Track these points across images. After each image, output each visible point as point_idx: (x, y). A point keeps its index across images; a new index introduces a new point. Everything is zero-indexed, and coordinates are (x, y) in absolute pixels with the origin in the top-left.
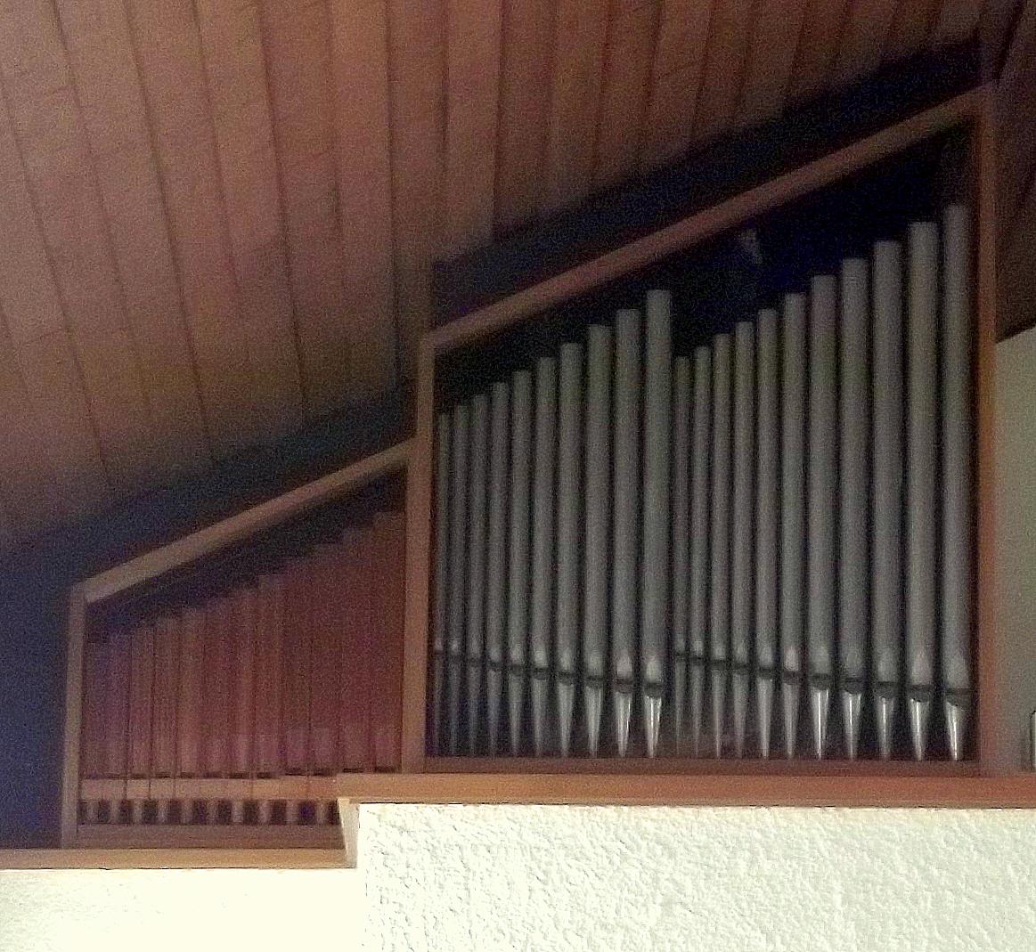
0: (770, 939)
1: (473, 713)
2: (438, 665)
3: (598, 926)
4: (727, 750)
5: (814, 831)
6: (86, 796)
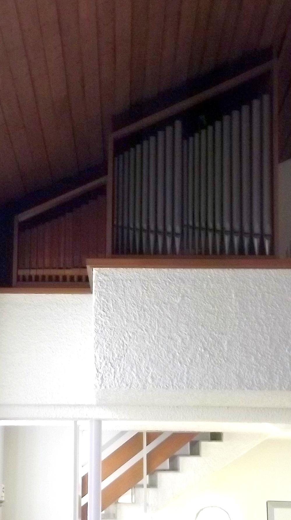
0: (213, 307)
1: (125, 239)
2: (115, 229)
3: (163, 303)
4: (200, 253)
5: (226, 276)
6: (19, 274)
